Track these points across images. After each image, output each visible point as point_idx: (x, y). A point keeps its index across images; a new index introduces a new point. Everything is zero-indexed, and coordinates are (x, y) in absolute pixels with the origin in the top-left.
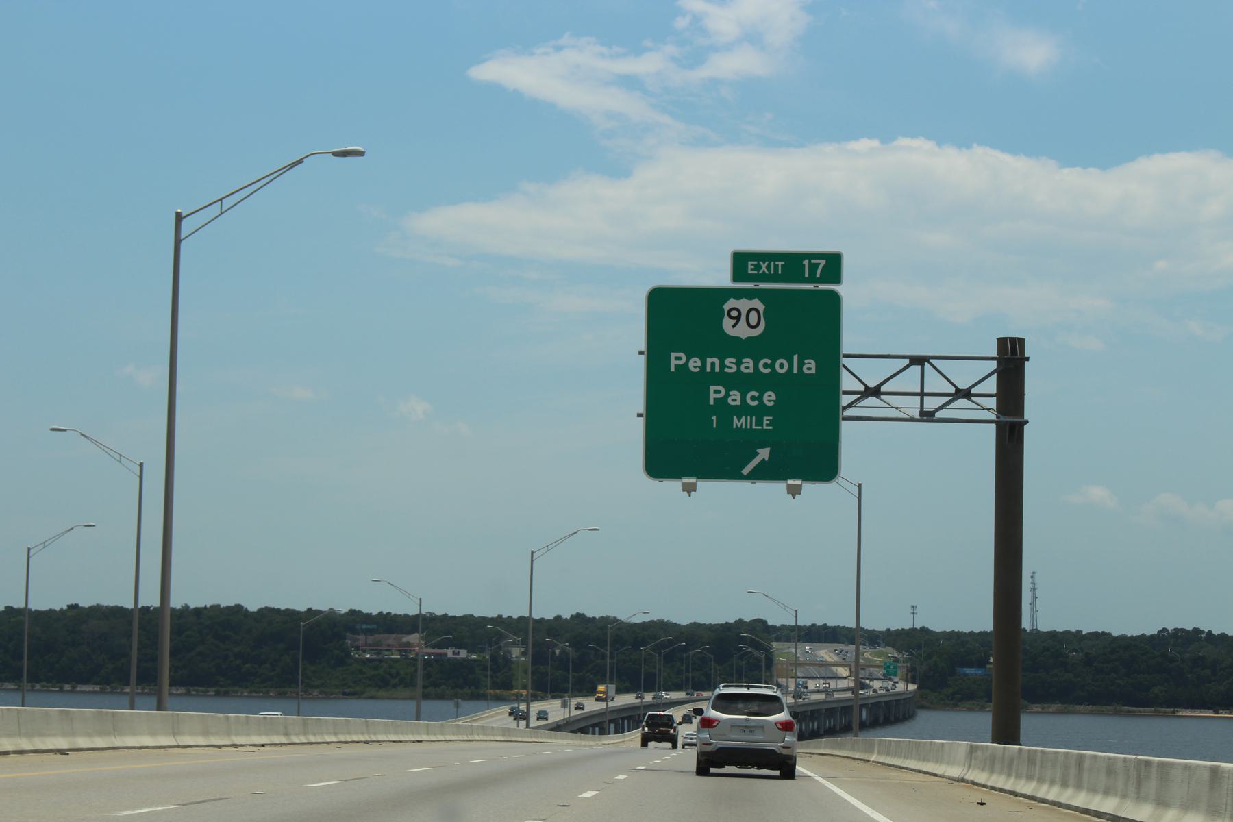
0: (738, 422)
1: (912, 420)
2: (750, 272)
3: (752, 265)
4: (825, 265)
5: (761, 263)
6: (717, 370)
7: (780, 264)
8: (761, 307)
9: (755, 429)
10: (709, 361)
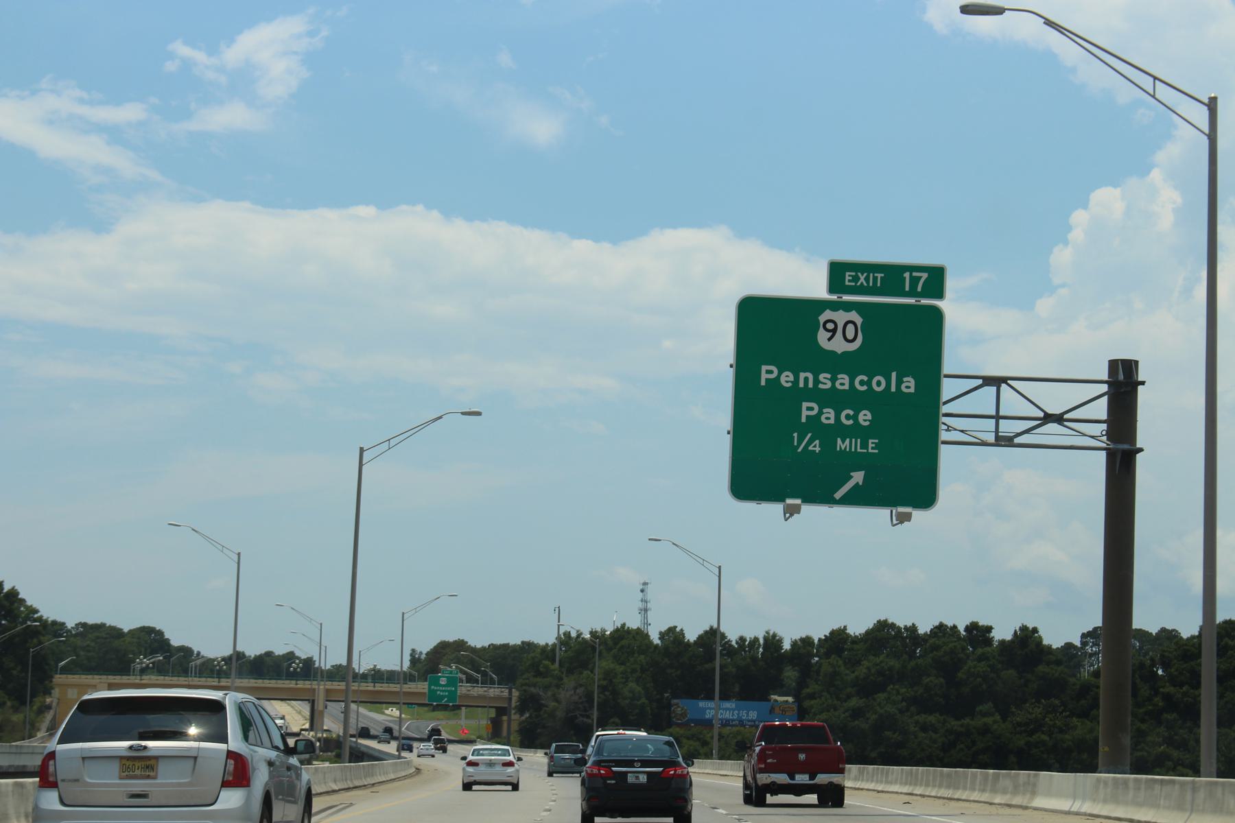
0: (842, 445)
1: (984, 444)
2: (847, 283)
3: (849, 276)
4: (927, 278)
5: (859, 274)
6: (811, 385)
7: (879, 275)
8: (859, 320)
9: (860, 452)
10: (802, 375)
